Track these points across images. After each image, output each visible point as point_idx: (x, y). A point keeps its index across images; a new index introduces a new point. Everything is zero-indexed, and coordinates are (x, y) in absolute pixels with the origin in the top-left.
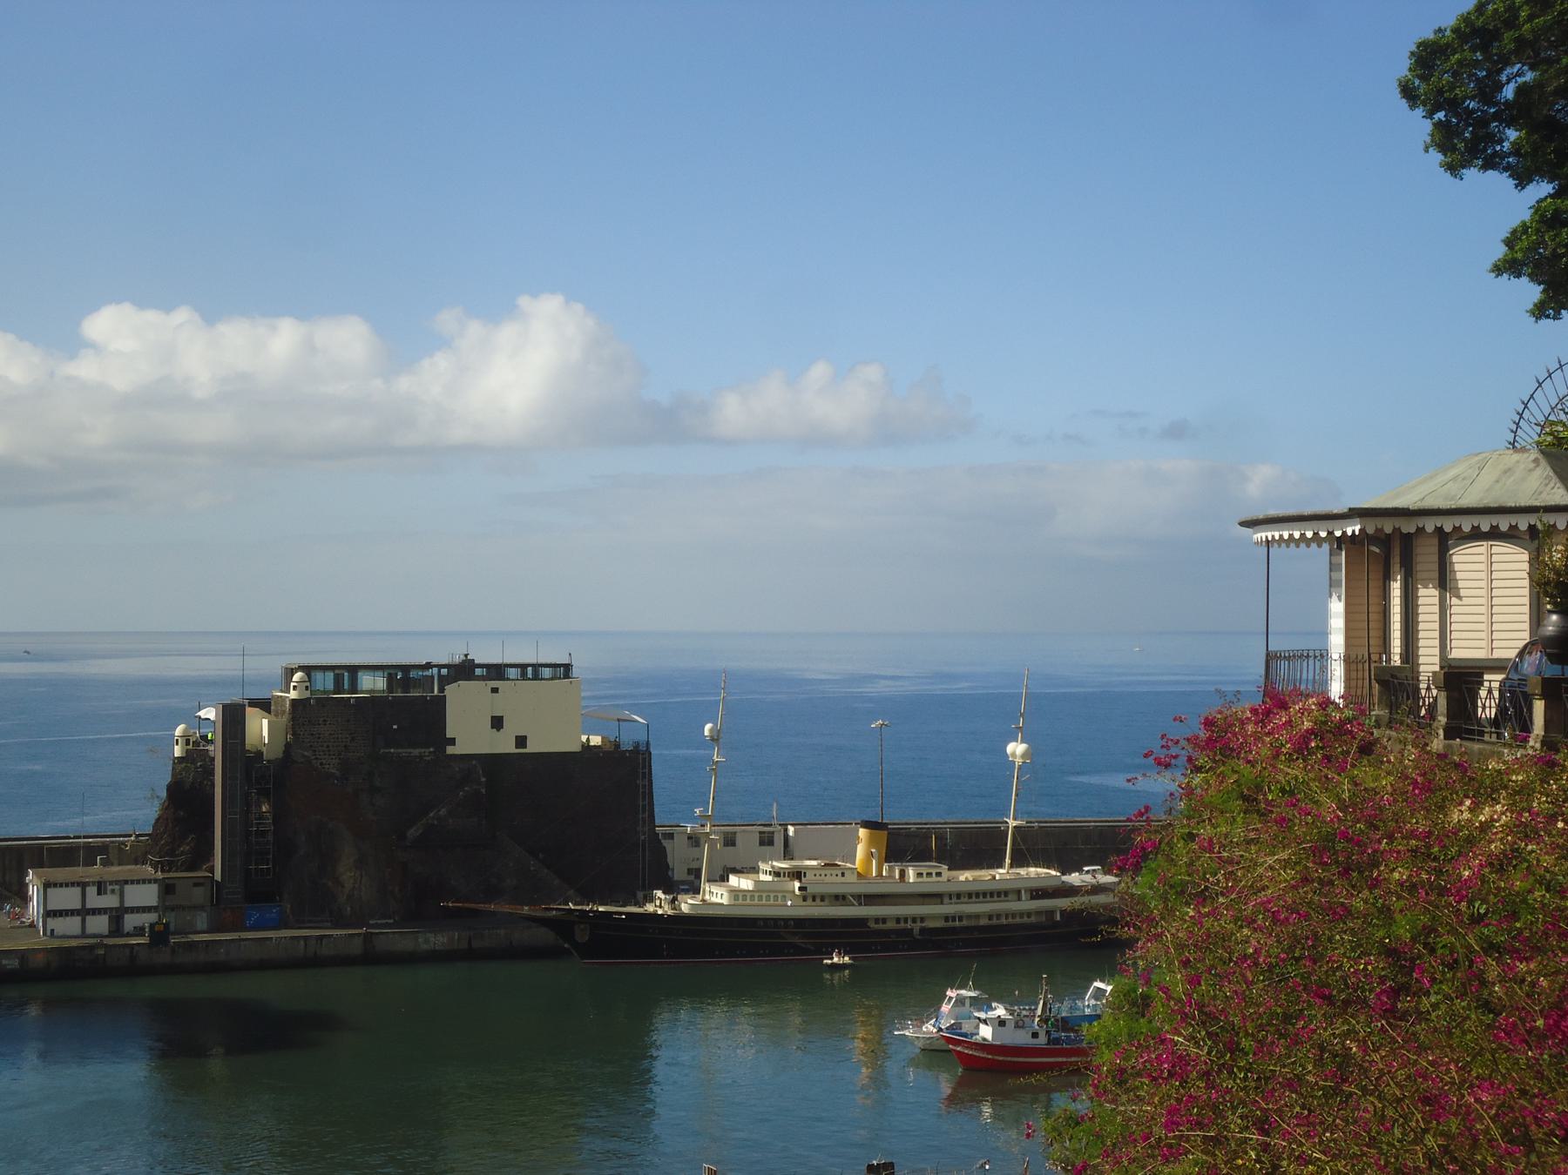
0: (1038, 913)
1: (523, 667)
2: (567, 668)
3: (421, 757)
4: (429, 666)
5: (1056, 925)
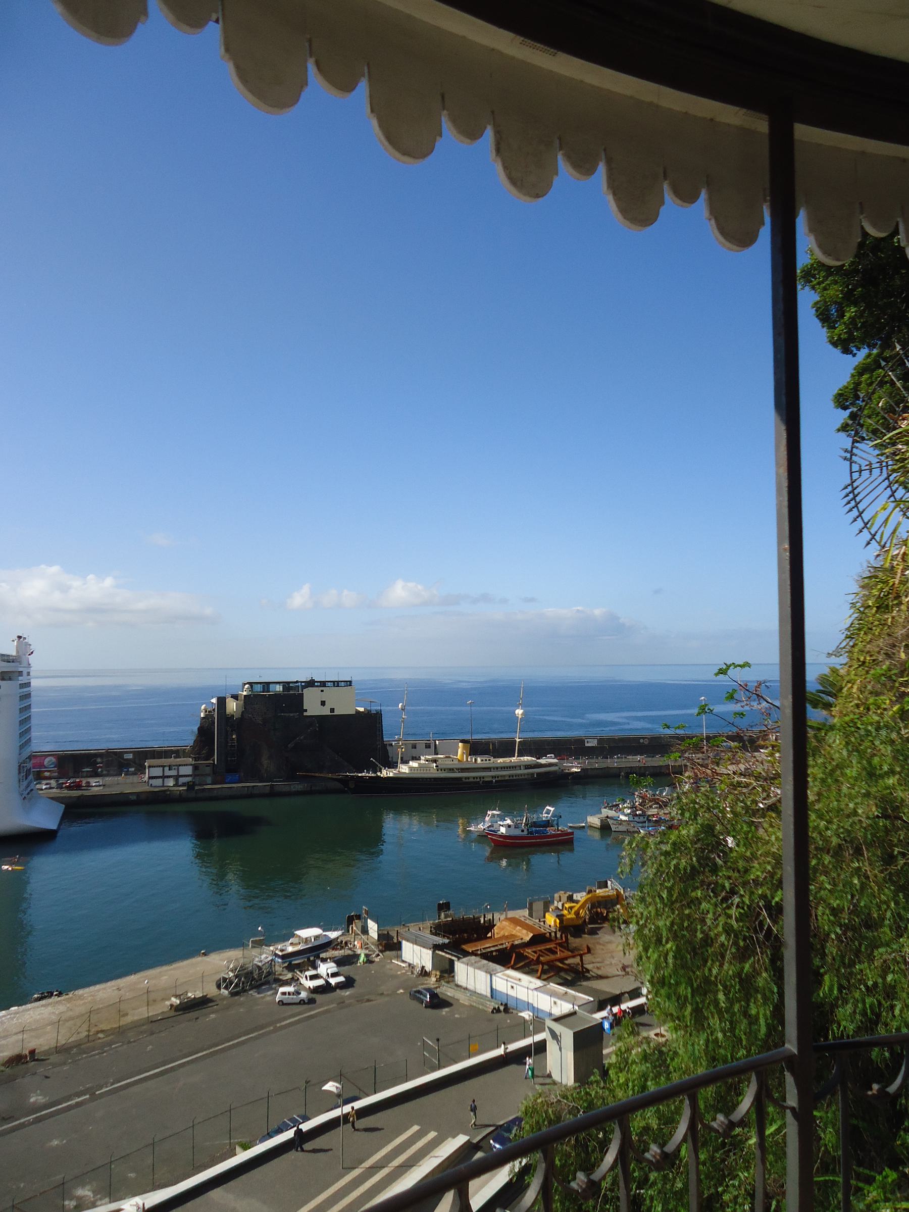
0: (528, 774)
1: (334, 682)
2: (350, 682)
3: (294, 716)
4: (297, 682)
5: (536, 779)
